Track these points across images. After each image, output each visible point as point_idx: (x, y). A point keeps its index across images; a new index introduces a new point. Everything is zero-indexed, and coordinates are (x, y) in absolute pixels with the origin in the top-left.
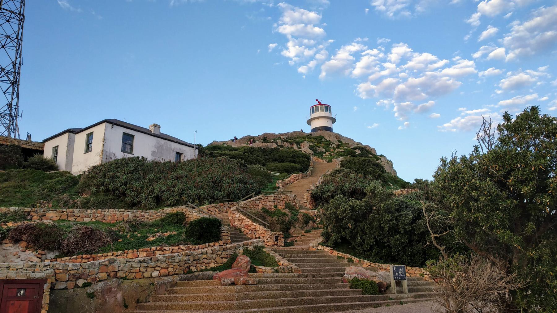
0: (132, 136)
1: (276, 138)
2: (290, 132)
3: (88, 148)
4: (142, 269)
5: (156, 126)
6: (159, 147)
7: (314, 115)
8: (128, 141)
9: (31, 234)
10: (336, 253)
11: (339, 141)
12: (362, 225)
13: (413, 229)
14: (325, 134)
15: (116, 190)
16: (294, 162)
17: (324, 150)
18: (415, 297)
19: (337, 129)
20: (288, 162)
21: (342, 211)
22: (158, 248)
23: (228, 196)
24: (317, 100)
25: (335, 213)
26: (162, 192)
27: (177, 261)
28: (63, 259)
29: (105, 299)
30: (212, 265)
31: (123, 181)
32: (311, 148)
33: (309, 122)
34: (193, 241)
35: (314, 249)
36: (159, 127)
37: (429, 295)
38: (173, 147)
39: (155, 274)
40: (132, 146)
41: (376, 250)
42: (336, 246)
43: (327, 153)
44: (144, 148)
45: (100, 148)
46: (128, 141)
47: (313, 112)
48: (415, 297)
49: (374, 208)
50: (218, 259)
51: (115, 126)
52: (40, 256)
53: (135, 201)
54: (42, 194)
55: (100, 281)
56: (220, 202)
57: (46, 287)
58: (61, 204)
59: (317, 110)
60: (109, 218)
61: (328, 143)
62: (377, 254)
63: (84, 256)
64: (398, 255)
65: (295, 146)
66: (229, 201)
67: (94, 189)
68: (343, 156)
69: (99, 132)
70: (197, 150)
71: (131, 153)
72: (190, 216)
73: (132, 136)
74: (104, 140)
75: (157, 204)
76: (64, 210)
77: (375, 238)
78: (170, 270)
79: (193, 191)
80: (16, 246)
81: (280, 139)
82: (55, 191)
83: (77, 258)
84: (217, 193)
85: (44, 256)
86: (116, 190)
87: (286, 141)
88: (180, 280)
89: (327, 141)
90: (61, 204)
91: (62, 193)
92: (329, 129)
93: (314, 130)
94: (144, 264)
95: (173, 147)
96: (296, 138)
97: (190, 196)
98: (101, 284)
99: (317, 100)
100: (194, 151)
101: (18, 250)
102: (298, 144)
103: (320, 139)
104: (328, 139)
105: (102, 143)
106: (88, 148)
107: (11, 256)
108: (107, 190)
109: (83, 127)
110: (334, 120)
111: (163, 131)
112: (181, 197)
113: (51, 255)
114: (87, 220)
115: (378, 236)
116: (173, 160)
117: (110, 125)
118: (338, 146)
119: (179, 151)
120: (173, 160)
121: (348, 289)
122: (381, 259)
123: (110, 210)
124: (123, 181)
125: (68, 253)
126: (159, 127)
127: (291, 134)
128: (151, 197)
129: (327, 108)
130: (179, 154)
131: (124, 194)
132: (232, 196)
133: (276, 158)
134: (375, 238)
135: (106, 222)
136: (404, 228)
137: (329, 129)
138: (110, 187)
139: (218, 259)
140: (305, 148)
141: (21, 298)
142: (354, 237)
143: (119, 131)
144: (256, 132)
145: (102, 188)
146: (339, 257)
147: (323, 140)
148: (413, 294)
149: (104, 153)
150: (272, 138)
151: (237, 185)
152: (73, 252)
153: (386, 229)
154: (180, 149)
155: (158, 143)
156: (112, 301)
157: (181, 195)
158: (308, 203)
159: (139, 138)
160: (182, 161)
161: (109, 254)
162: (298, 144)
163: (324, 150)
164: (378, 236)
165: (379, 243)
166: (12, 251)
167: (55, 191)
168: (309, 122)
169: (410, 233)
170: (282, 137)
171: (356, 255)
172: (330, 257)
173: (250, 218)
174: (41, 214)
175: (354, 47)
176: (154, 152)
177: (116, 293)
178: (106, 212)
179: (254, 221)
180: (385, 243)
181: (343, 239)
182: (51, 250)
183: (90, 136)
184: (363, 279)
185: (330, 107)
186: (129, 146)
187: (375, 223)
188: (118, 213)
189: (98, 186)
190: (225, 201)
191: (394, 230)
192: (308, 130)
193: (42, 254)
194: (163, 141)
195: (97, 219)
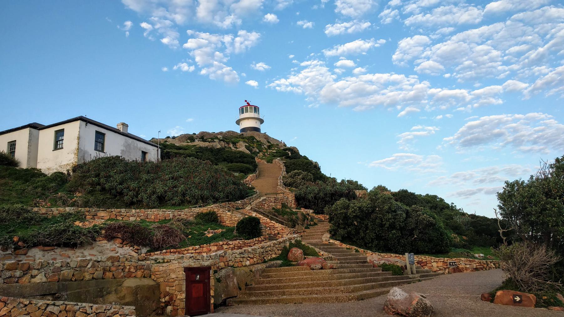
0: (104, 135)
1: (213, 137)
2: (224, 131)
3: (57, 146)
4: (241, 260)
5: (125, 125)
6: (128, 146)
7: (243, 116)
8: (100, 138)
9: (125, 232)
10: (344, 246)
11: (269, 142)
12: (365, 223)
13: (406, 226)
14: (255, 134)
15: (113, 189)
16: (243, 162)
17: (258, 151)
18: (421, 276)
19: (264, 129)
20: (237, 162)
21: (352, 211)
22: (225, 243)
23: (227, 197)
24: (246, 101)
25: (346, 214)
26: (166, 192)
27: (258, 252)
28: (156, 253)
29: (227, 282)
30: (274, 256)
31: (118, 181)
32: (247, 148)
33: (238, 122)
34: (245, 236)
35: (327, 243)
36: (127, 126)
37: (427, 276)
38: (139, 146)
39: (248, 263)
40: (103, 144)
41: (376, 242)
42: (343, 240)
43: (261, 154)
44: (114, 147)
45: (75, 146)
46: (100, 138)
47: (243, 113)
48: (421, 276)
49: (377, 209)
50: (276, 251)
51: (88, 124)
52: (136, 251)
53: (135, 200)
54: (37, 193)
55: (222, 269)
56: (222, 202)
57: (211, 272)
58: (60, 203)
59: (247, 111)
60: (153, 217)
61: (260, 144)
62: (376, 246)
63: (172, 250)
64: (394, 246)
65: (231, 145)
66: (227, 201)
67: (89, 188)
68: (280, 157)
69: (72, 131)
70: (159, 150)
71: (102, 150)
72: (222, 215)
73: (104, 135)
74: (79, 138)
75: (160, 204)
76: (113, 210)
77: (375, 233)
78: (255, 259)
79: (197, 192)
80: (110, 243)
81: (217, 138)
82: (48, 189)
83: (166, 252)
84: (217, 194)
85: (139, 251)
86: (113, 189)
87: (224, 141)
88: (266, 267)
89: (258, 142)
90: (60, 203)
91: (56, 192)
92: (257, 130)
93: (243, 130)
94: (242, 256)
95: (139, 146)
96: (229, 138)
97: (194, 197)
98: (223, 271)
99: (246, 101)
100: (158, 150)
101: (114, 246)
102: (234, 144)
103: (252, 139)
104: (258, 139)
105: (76, 141)
106: (57, 146)
107: (108, 252)
108: (103, 189)
109: (46, 124)
110: (262, 121)
111: (130, 131)
112: (184, 197)
113: (144, 250)
114: (132, 219)
115: (378, 231)
116: (139, 159)
117: (84, 123)
118: (269, 147)
119: (144, 151)
120: (139, 159)
121: (381, 272)
122: (379, 250)
123: (153, 210)
124: (118, 181)
125: (159, 248)
126: (127, 126)
127: (226, 133)
128: (154, 197)
129: (256, 109)
130: (144, 153)
131: (121, 194)
132: (230, 197)
133: (225, 159)
134: (375, 233)
135: (150, 220)
136: (400, 225)
137: (257, 130)
138: (107, 186)
139: (276, 251)
140: (242, 147)
141: (198, 282)
142: (358, 233)
143: (93, 129)
144: (196, 130)
145: (98, 187)
146: (347, 248)
147: (255, 140)
148: (419, 275)
149: (80, 151)
150: (208, 137)
151: (232, 187)
152: (162, 247)
153: (387, 225)
154: (145, 148)
155: (126, 142)
156: (231, 284)
157: (184, 195)
158: (293, 203)
159: (109, 137)
160: (147, 160)
161: (191, 248)
162: (234, 144)
163: (258, 151)
164: (378, 231)
165: (378, 237)
166: (108, 247)
167: (48, 189)
168: (238, 122)
169: (402, 229)
170: (219, 136)
171: (360, 247)
172: (339, 248)
173: (267, 216)
174: (93, 213)
175: (363, 70)
176: (123, 150)
177: (233, 278)
178: (149, 211)
179: (271, 219)
180: (383, 236)
181: (349, 233)
182: (145, 246)
183: (59, 134)
184: (390, 264)
185: (258, 108)
186: (101, 145)
187: (377, 221)
188: (161, 213)
189: (92, 184)
190: (225, 201)
191: (392, 227)
192: (237, 129)
193: (138, 250)
194: (130, 140)
195: (141, 218)
